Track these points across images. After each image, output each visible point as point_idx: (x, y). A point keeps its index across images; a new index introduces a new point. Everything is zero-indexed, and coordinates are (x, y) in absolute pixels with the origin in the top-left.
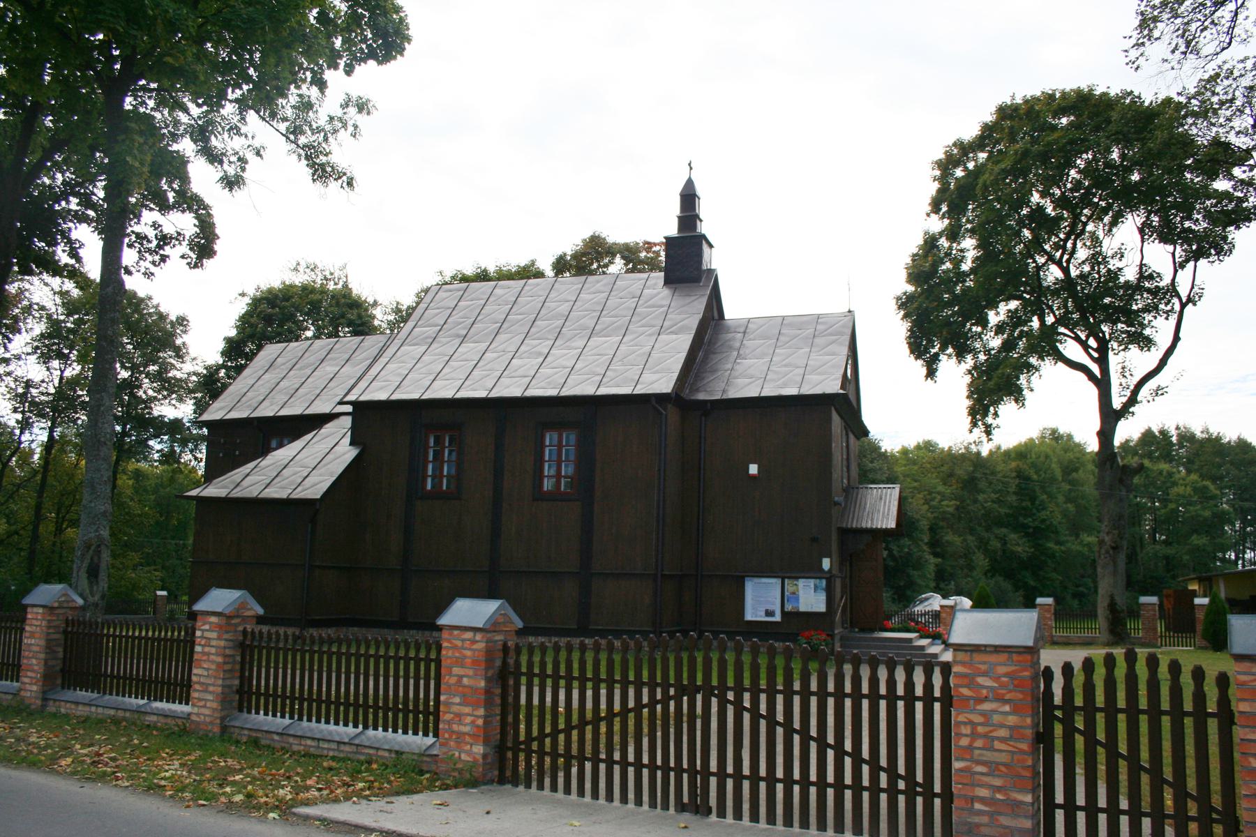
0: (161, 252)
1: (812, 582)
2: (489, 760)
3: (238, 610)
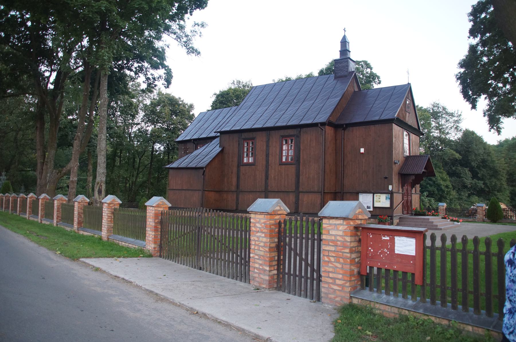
0: (154, 84)
2: (157, 249)
3: (112, 201)
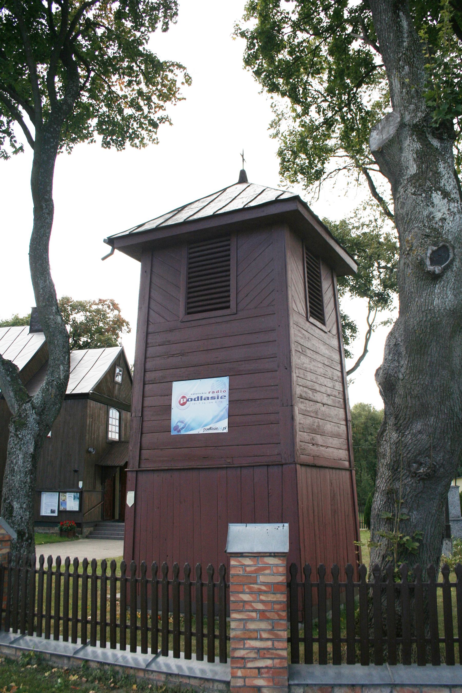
1: (72, 495)
